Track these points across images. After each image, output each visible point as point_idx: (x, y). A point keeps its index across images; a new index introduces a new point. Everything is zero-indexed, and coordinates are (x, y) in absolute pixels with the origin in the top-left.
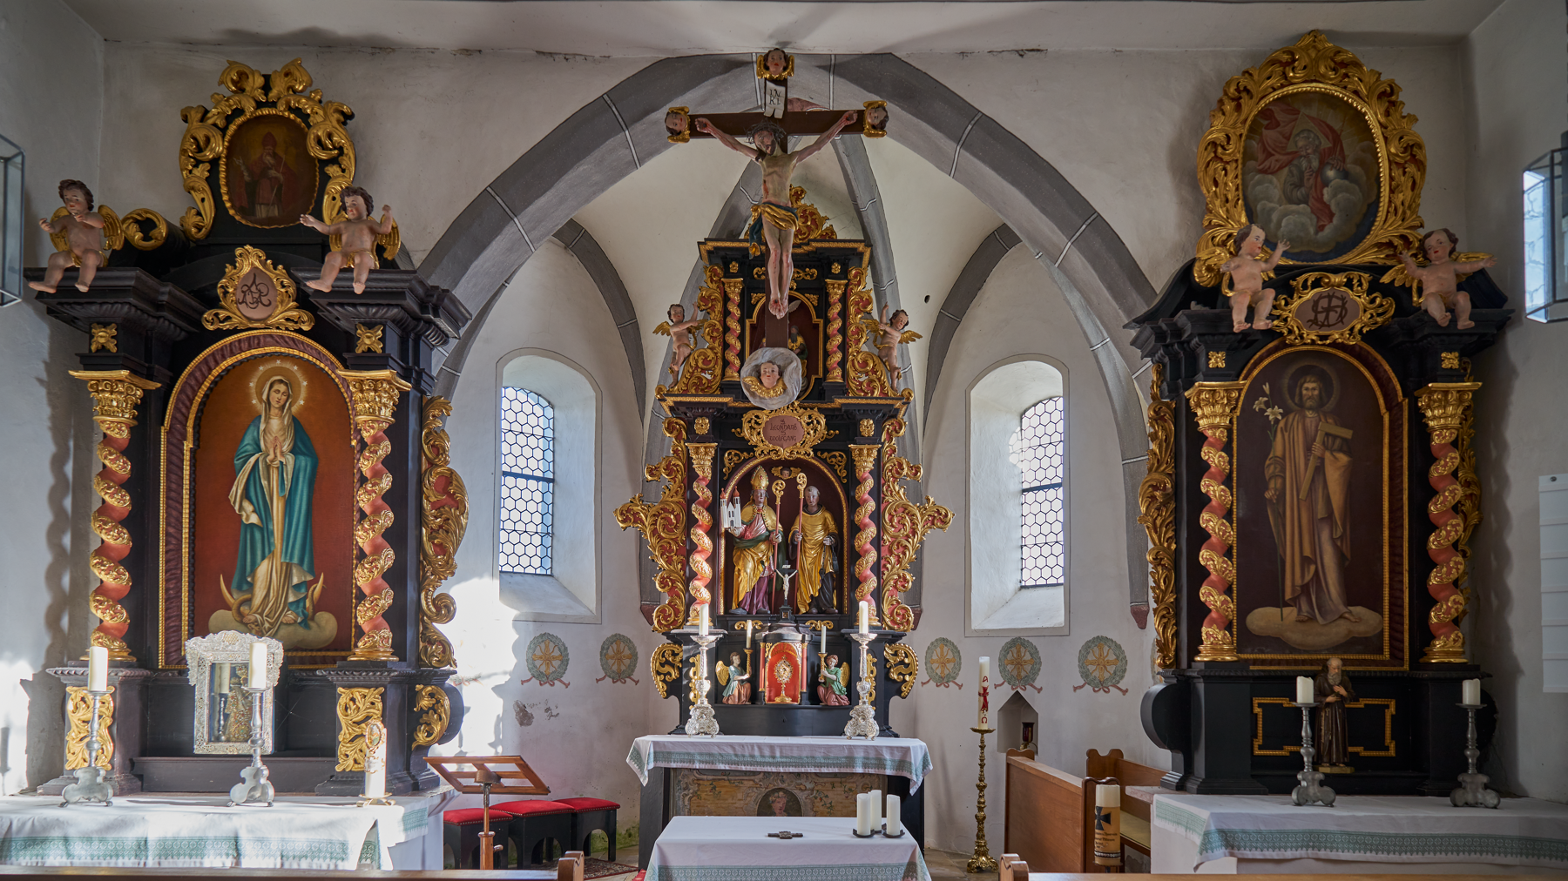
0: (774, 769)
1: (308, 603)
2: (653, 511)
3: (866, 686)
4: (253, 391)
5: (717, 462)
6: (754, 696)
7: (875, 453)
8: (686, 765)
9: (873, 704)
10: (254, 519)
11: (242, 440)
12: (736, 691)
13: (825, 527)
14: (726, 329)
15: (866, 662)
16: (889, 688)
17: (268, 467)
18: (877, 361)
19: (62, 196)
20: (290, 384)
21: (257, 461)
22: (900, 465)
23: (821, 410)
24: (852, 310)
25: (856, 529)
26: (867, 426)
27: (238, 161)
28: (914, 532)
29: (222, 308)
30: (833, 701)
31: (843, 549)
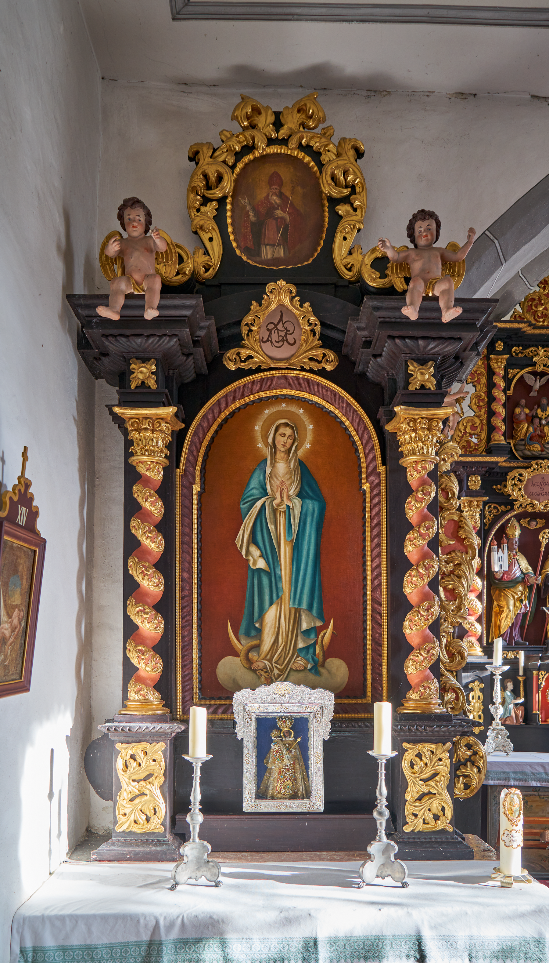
1: (318, 649)
4: (258, 434)
10: (261, 564)
11: (248, 484)
17: (275, 511)
19: (120, 217)
20: (296, 427)
21: (264, 505)
27: (244, 201)
29: (243, 347)
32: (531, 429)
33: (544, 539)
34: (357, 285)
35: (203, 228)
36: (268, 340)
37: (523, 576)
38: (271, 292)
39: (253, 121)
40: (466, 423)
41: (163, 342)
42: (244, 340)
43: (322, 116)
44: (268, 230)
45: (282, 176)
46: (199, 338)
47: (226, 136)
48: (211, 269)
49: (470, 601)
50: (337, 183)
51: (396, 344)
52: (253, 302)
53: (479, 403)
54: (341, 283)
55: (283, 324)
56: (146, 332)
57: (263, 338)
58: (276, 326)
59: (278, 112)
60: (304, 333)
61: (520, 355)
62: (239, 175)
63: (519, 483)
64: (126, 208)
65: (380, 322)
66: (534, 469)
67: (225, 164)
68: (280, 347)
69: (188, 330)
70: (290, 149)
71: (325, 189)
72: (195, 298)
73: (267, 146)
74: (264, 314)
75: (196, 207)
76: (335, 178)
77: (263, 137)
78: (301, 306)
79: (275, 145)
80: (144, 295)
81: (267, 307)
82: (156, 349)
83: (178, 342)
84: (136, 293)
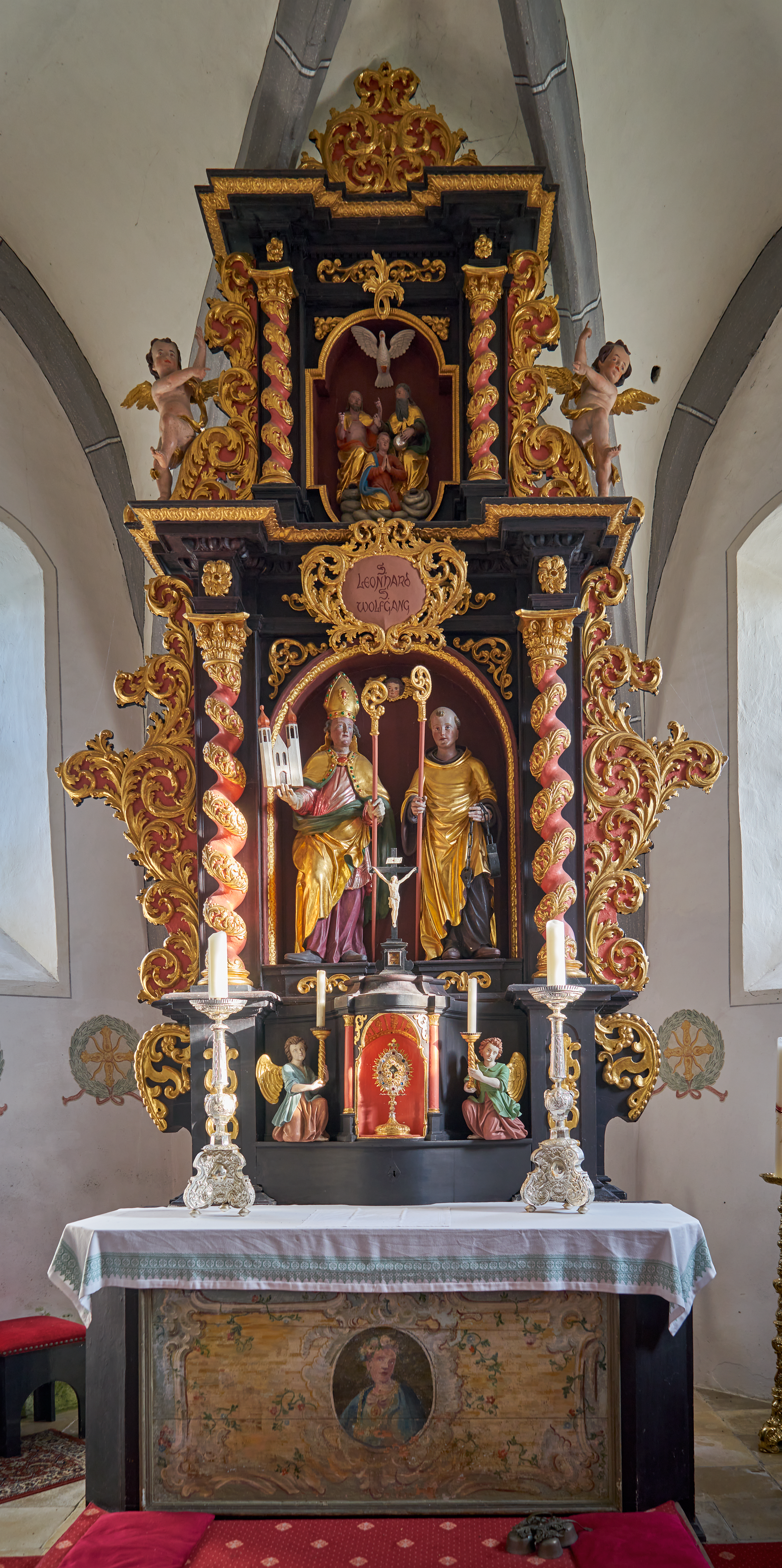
0: (368, 1287)
2: (132, 764)
3: (562, 1098)
5: (253, 660)
6: (335, 1125)
7: (568, 630)
8: (172, 1282)
9: (574, 1134)
12: (297, 1111)
13: (472, 790)
14: (264, 381)
15: (561, 1052)
16: (606, 1101)
18: (570, 443)
22: (618, 662)
23: (458, 543)
24: (518, 338)
25: (532, 786)
26: (554, 572)
28: (647, 795)
30: (494, 1131)
31: (508, 830)
32: (371, 460)
33: (372, 707)
37: (359, 804)
40: (208, 443)
49: (212, 859)
53: (236, 392)
61: (337, 279)
63: (327, 581)
66: (359, 544)
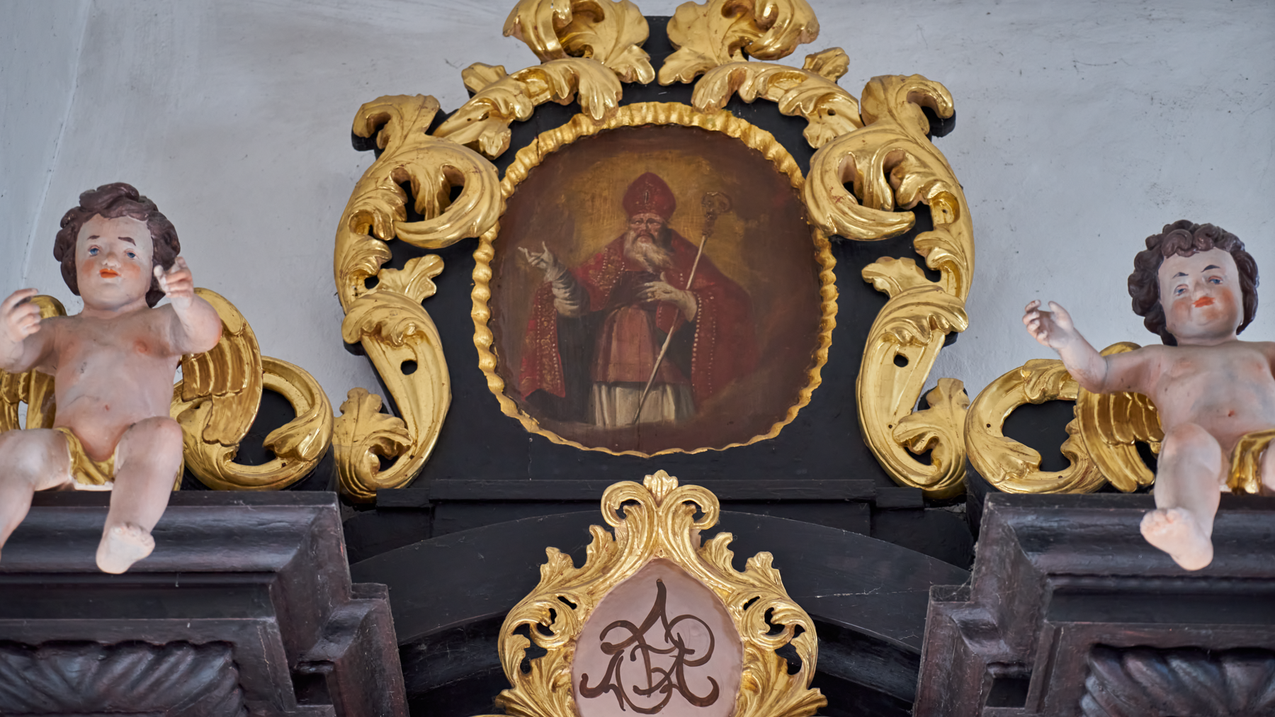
19: (65, 248)
27: (536, 257)
34: (957, 509)
35: (384, 333)
36: (604, 687)
38: (620, 514)
39: (574, 38)
41: (171, 670)
42: (509, 686)
43: (804, 22)
44: (619, 340)
45: (670, 185)
46: (326, 669)
47: (483, 80)
48: (403, 460)
50: (866, 198)
51: (1129, 675)
52: (552, 552)
54: (888, 499)
55: (668, 627)
56: (107, 630)
57: (585, 677)
58: (638, 634)
59: (659, 18)
60: (754, 658)
62: (521, 185)
64: (87, 219)
65: (1058, 593)
67: (478, 150)
68: (655, 710)
69: (272, 620)
70: (699, 110)
71: (823, 214)
72: (308, 502)
73: (621, 104)
74: (591, 593)
75: (362, 273)
76: (856, 185)
77: (605, 76)
78: (739, 564)
79: (648, 101)
80: (109, 493)
81: (605, 569)
82: (143, 697)
83: (233, 674)
84: (82, 485)
